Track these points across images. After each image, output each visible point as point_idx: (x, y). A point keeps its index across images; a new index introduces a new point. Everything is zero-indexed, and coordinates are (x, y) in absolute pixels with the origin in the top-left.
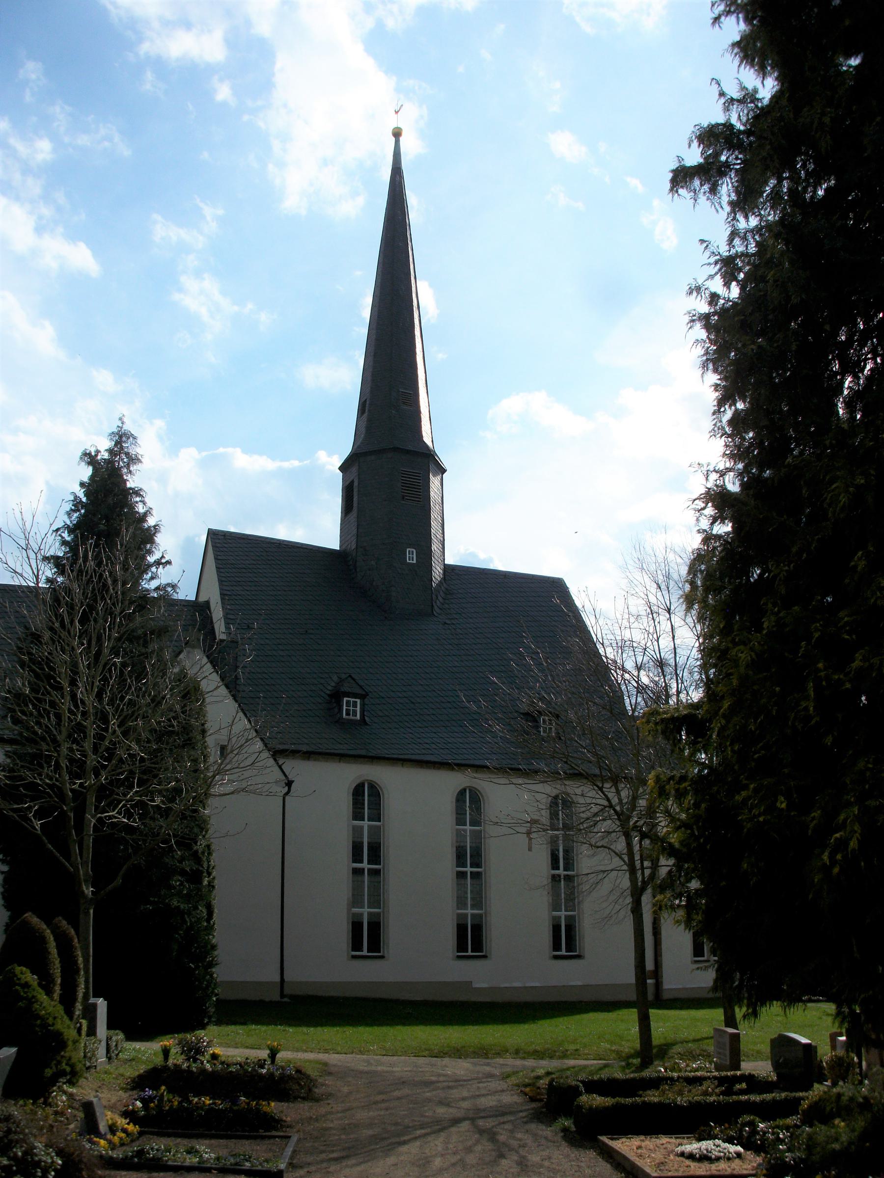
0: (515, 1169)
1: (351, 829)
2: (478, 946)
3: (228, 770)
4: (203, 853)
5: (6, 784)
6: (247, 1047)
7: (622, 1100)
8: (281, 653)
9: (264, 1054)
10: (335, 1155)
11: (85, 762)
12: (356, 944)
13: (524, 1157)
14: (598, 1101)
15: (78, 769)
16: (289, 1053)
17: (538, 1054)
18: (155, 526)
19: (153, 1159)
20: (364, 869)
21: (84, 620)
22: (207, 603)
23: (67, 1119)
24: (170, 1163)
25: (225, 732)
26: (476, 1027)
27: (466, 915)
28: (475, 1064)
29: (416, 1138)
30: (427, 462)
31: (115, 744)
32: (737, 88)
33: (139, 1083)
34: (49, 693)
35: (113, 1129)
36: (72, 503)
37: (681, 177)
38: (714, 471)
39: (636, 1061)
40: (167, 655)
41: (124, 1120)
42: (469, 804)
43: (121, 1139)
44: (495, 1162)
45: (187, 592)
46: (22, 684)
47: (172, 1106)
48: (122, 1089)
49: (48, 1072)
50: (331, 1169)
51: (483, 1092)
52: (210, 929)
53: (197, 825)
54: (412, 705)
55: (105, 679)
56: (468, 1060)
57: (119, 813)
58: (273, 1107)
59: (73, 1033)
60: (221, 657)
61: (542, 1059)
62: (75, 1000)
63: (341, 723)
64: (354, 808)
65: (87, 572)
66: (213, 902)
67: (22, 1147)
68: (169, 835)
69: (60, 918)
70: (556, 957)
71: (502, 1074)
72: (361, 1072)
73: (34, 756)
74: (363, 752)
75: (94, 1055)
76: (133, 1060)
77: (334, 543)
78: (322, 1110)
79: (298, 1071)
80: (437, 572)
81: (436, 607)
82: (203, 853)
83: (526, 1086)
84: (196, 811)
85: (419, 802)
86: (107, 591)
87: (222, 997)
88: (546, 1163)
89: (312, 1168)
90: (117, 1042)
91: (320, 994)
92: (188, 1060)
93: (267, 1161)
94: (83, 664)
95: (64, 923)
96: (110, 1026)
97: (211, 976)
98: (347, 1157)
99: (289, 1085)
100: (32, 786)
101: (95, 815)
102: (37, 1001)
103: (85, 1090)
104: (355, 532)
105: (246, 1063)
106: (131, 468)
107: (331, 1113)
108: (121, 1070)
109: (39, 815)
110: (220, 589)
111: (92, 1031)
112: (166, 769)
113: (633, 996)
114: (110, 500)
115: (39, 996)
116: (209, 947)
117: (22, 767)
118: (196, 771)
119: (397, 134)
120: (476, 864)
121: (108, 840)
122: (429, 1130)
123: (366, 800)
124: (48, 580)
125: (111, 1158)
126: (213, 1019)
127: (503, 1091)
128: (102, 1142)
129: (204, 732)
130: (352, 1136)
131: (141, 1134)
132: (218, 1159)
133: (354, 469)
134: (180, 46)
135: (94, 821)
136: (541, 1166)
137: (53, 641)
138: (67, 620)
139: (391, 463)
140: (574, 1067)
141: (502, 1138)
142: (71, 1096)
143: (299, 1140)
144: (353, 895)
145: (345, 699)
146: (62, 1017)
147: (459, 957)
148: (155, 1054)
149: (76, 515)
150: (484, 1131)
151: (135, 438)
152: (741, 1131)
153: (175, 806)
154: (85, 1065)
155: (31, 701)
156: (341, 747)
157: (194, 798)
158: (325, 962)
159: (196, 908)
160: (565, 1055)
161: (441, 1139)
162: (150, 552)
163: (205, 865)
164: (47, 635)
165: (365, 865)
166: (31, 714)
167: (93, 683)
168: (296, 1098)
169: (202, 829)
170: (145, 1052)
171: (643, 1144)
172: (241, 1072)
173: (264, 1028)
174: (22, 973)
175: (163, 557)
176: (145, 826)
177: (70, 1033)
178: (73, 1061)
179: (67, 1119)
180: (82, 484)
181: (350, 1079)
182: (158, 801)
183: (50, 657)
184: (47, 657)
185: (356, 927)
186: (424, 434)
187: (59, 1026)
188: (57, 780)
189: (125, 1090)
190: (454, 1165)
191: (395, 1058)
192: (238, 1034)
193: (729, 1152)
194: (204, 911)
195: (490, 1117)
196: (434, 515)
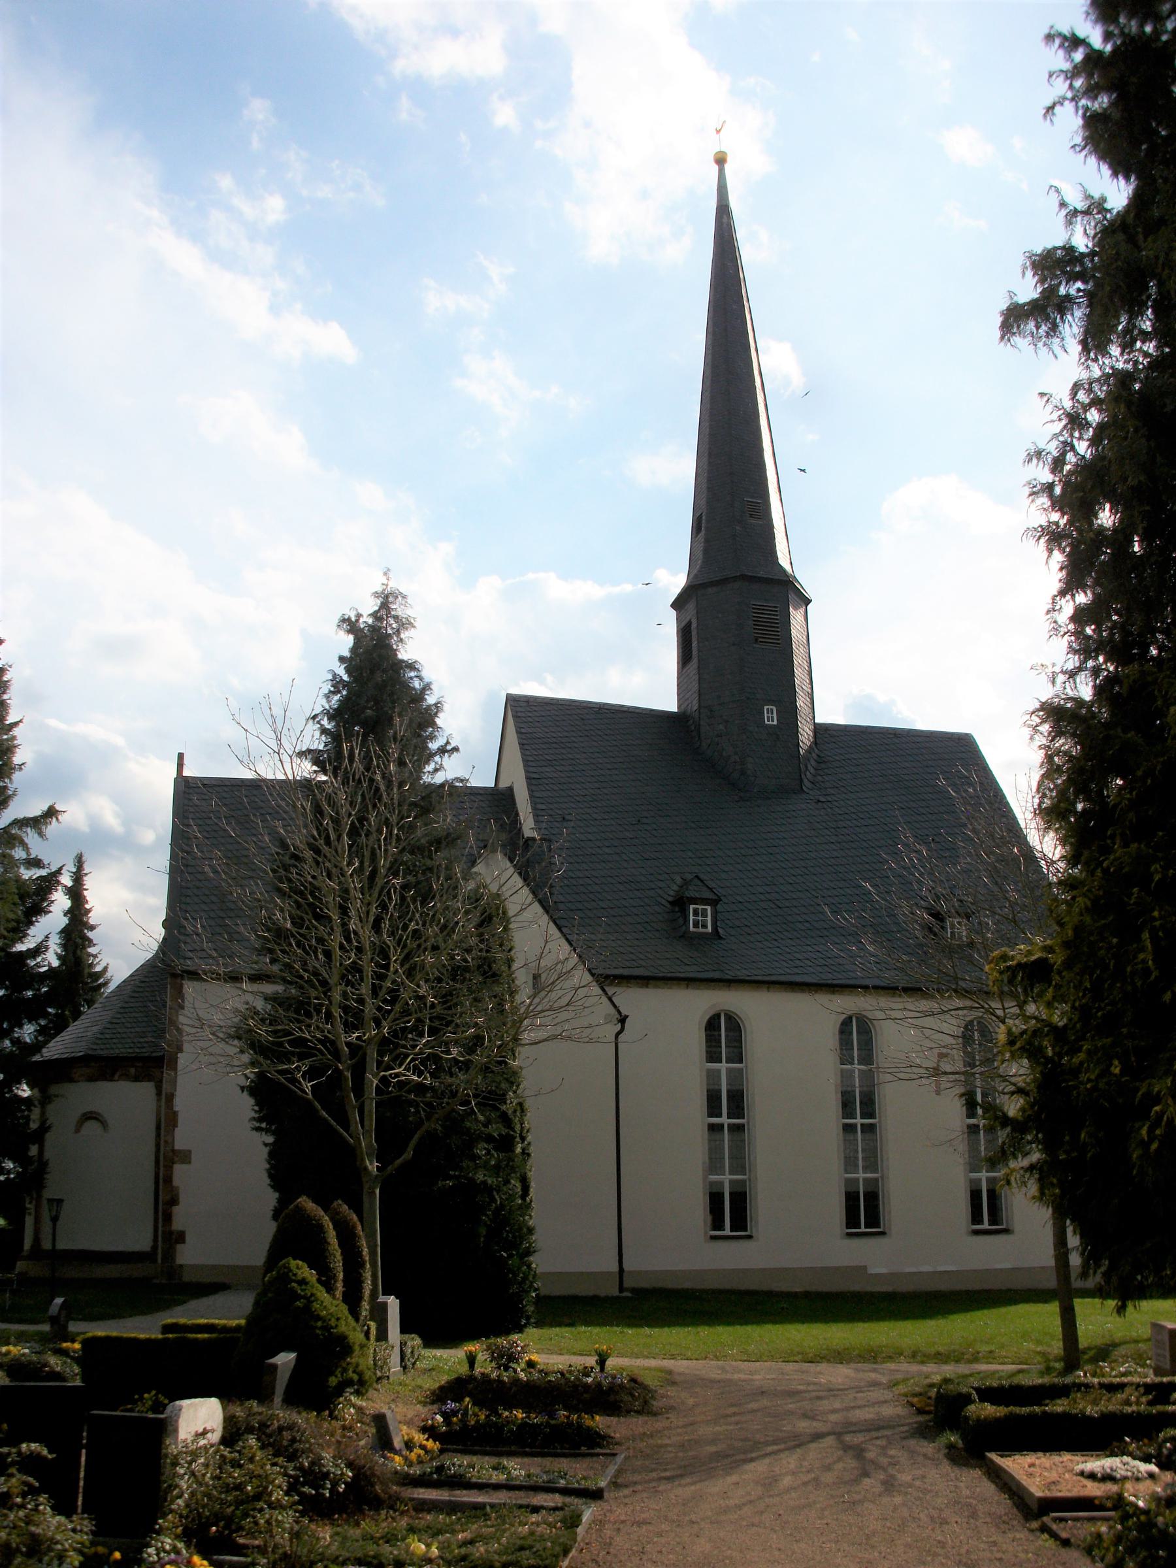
0: (879, 1489)
1: (704, 1073)
2: (874, 1219)
4: (515, 1111)
5: (268, 1042)
6: (574, 1354)
7: (1017, 1410)
8: (607, 850)
9: (591, 1361)
10: (668, 1474)
11: (363, 1011)
13: (892, 1476)
14: (989, 1410)
15: (354, 1020)
17: (940, 1358)
18: (436, 704)
19: (454, 1476)
20: (722, 1126)
21: (354, 832)
22: (510, 789)
23: (357, 1434)
24: (474, 1480)
26: (866, 1325)
27: (857, 1180)
28: (857, 1370)
29: (766, 1455)
30: (784, 592)
32: (1080, 196)
33: (440, 1396)
35: (409, 1445)
36: (330, 683)
37: (1015, 318)
38: (1062, 672)
39: (1059, 1365)
42: (856, 1037)
43: (419, 1456)
44: (856, 1481)
45: (483, 778)
47: (478, 1421)
48: (420, 1402)
49: (333, 1381)
50: (660, 1488)
51: (860, 1403)
54: (779, 910)
56: (853, 1365)
57: (407, 1069)
58: (599, 1422)
59: (361, 1337)
60: (527, 859)
61: (946, 1363)
62: (360, 1298)
66: (529, 1174)
67: (308, 1457)
68: (468, 1095)
69: (340, 1202)
70: (977, 1233)
71: (890, 1381)
72: (712, 1381)
74: (717, 975)
75: (385, 1363)
76: (433, 1369)
77: (668, 702)
78: (666, 1423)
79: (633, 1380)
80: (806, 735)
81: (805, 781)
82: (515, 1111)
83: (915, 1395)
85: (790, 1037)
86: (380, 799)
87: (544, 1292)
88: (918, 1483)
89: (639, 1487)
90: (413, 1348)
91: (660, 1285)
93: (585, 1478)
94: (355, 884)
95: (345, 1207)
96: (403, 1330)
97: (529, 1266)
98: (681, 1476)
99: (615, 1397)
100: (301, 1042)
101: (378, 1074)
102: (317, 1300)
103: (376, 1402)
105: (570, 1372)
106: (402, 636)
107: (669, 1428)
108: (419, 1381)
109: (310, 1074)
110: (526, 771)
111: (382, 1335)
113: (1051, 1282)
115: (319, 1294)
119: (721, 160)
120: (869, 1112)
121: (394, 1104)
122: (782, 1446)
123: (724, 1036)
125: (408, 1474)
126: (532, 1320)
127: (885, 1402)
128: (397, 1458)
130: (690, 1454)
131: (442, 1451)
132: (529, 1476)
133: (691, 607)
134: (442, 60)
135: (376, 1082)
136: (910, 1486)
137: (318, 863)
139: (739, 596)
140: (979, 1373)
141: (870, 1455)
142: (360, 1410)
143: (626, 1458)
144: (710, 1159)
145: (692, 907)
146: (347, 1318)
147: (849, 1235)
148: (459, 1363)
149: (337, 697)
150: (850, 1447)
151: (404, 597)
152: (1160, 1447)
153: (475, 1058)
154: (375, 1374)
155: (293, 936)
156: (687, 968)
157: (499, 1047)
158: (678, 1245)
159: (507, 1182)
160: (975, 1359)
161: (795, 1457)
162: (432, 737)
163: (518, 1128)
165: (724, 1120)
168: (628, 1412)
169: (512, 1083)
170: (447, 1360)
171: (1037, 1462)
172: (563, 1381)
173: (596, 1330)
175: (448, 743)
177: (356, 1337)
178: (360, 1368)
180: (342, 659)
181: (698, 1390)
183: (315, 882)
184: (311, 883)
186: (779, 554)
187: (343, 1328)
189: (424, 1404)
190: (805, 1484)
191: (758, 1364)
192: (564, 1337)
193: (1139, 1471)
194: (518, 1185)
195: (860, 1431)
196: (798, 660)
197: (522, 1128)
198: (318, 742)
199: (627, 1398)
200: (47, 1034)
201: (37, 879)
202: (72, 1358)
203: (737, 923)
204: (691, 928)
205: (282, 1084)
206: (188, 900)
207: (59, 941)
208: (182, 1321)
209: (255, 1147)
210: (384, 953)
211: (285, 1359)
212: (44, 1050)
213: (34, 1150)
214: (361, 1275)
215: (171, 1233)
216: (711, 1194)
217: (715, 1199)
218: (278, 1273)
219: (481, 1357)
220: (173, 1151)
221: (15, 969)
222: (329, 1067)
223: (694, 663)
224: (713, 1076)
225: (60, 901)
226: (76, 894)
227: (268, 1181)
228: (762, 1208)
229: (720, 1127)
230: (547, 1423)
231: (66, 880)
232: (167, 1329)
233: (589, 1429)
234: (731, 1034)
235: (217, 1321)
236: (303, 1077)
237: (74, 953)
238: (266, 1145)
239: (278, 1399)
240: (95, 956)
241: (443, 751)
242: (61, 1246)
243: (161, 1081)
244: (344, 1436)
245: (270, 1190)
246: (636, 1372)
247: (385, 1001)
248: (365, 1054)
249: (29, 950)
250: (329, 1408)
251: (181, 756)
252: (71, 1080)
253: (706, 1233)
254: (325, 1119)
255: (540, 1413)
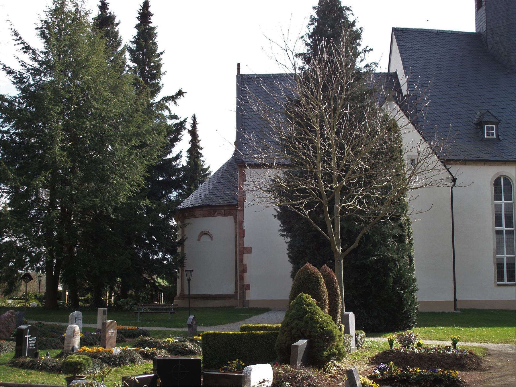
1: (494, 206)
3: (418, 173)
4: (405, 224)
6: (437, 340)
8: (444, 100)
9: (449, 343)
12: (500, 277)
16: (463, 343)
20: (503, 231)
22: (396, 73)
23: (338, 380)
25: (416, 150)
31: (349, 162)
33: (376, 360)
34: (308, 134)
40: (377, 106)
41: (370, 381)
45: (382, 68)
46: (291, 130)
48: (367, 364)
49: (326, 354)
52: (411, 270)
53: (401, 207)
55: (340, 124)
60: (406, 106)
62: (337, 313)
63: (483, 140)
64: (495, 193)
65: (324, 60)
66: (413, 254)
73: (302, 173)
74: (499, 158)
75: (349, 345)
78: (487, 376)
79: (470, 353)
82: (405, 224)
84: (399, 199)
86: (337, 70)
87: (420, 311)
90: (361, 337)
92: (404, 346)
96: (357, 328)
97: (414, 297)
103: (346, 364)
104: (485, 20)
107: (492, 378)
108: (365, 353)
109: (307, 207)
111: (347, 331)
112: (381, 175)
114: (333, 15)
115: (317, 311)
116: (411, 280)
117: (296, 179)
118: (398, 175)
121: (348, 218)
124: (301, 69)
129: (401, 151)
137: (308, 104)
138: (314, 90)
142: (338, 367)
145: (486, 126)
146: (332, 322)
153: (387, 197)
155: (297, 140)
156: (485, 155)
159: (402, 257)
164: (303, 101)
165: (504, 228)
166: (299, 148)
167: (333, 126)
168: (470, 369)
169: (404, 209)
172: (436, 354)
174: (306, 298)
176: (370, 210)
177: (336, 332)
179: (338, 380)
180: (314, 8)
182: (377, 194)
188: (316, 186)
189: (368, 364)
192: (431, 332)
197: (409, 232)
198: (304, 49)
199: (469, 362)
200: (182, 197)
201: (175, 124)
202: (199, 343)
203: (509, 133)
204: (494, 126)
205: (295, 212)
206: (246, 121)
207: (187, 155)
208: (250, 325)
209: (282, 244)
210: (341, 147)
211: (302, 343)
212: (182, 204)
213: (179, 249)
214: (337, 302)
215: (243, 285)
217: (499, 266)
218: (297, 300)
219: (396, 341)
220: (243, 248)
221: (167, 167)
222: (316, 202)
223: (483, 8)
224: (498, 208)
225: (186, 137)
226: (193, 133)
227: (288, 259)
230: (432, 374)
231: (188, 126)
232: (243, 329)
233: (453, 378)
234: (506, 187)
235: (267, 325)
236: (304, 208)
237: (194, 160)
238: (287, 243)
239: (299, 364)
240: (203, 161)
241: (365, 51)
242: (193, 292)
243: (237, 215)
244: (331, 381)
245: (289, 263)
246: (472, 349)
247: (342, 171)
248: (334, 196)
249: (173, 157)
250: (324, 367)
251: (239, 65)
252: (195, 217)
253: (495, 283)
254: (316, 228)
255: (428, 369)
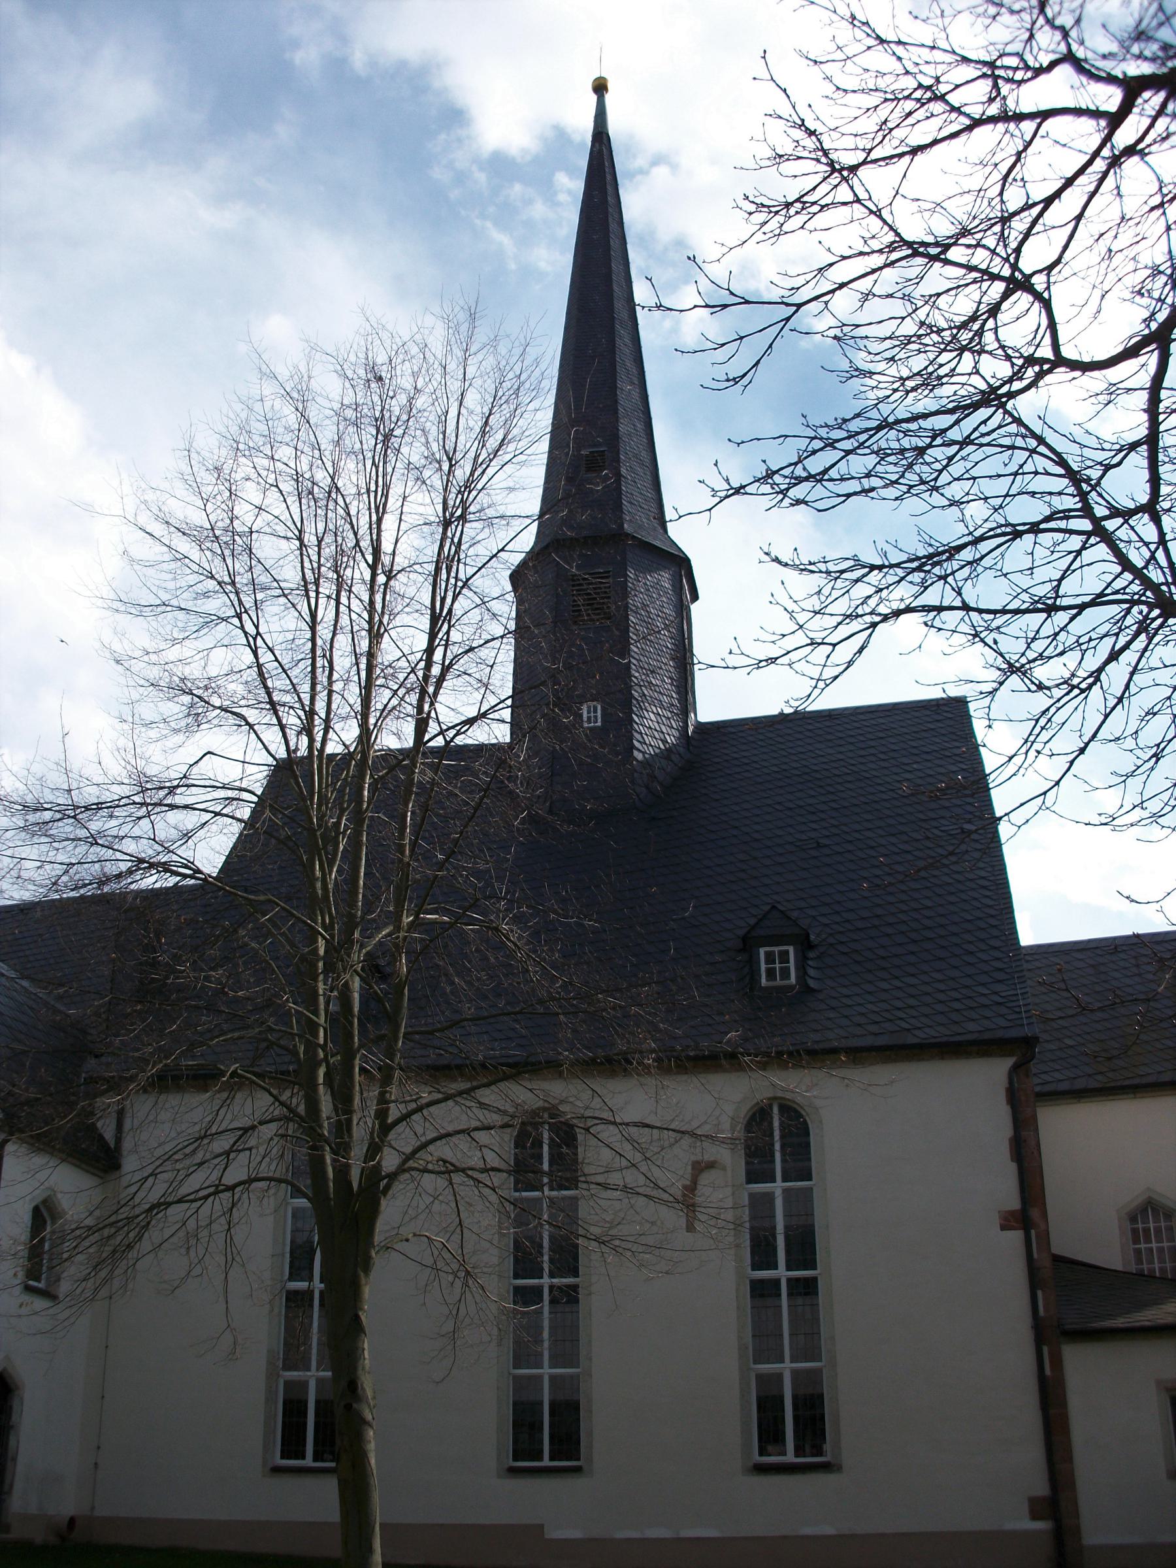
20: (776, 1282)
119: (600, 88)
123: (779, 1142)
145: (762, 951)
147: (277, 1470)
165: (782, 1272)
185: (768, 1407)
204: (791, 949)
216: (515, 1404)
224: (761, 1206)
228: (601, 1427)
229: (534, 1295)
